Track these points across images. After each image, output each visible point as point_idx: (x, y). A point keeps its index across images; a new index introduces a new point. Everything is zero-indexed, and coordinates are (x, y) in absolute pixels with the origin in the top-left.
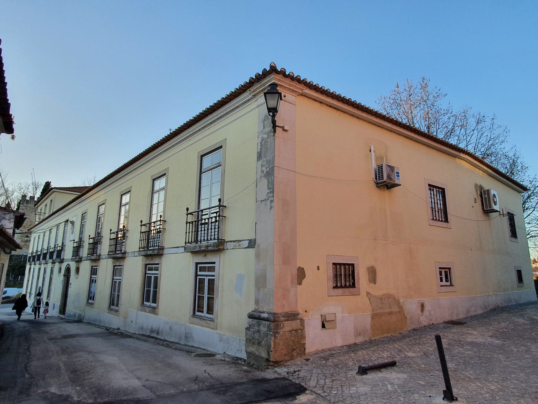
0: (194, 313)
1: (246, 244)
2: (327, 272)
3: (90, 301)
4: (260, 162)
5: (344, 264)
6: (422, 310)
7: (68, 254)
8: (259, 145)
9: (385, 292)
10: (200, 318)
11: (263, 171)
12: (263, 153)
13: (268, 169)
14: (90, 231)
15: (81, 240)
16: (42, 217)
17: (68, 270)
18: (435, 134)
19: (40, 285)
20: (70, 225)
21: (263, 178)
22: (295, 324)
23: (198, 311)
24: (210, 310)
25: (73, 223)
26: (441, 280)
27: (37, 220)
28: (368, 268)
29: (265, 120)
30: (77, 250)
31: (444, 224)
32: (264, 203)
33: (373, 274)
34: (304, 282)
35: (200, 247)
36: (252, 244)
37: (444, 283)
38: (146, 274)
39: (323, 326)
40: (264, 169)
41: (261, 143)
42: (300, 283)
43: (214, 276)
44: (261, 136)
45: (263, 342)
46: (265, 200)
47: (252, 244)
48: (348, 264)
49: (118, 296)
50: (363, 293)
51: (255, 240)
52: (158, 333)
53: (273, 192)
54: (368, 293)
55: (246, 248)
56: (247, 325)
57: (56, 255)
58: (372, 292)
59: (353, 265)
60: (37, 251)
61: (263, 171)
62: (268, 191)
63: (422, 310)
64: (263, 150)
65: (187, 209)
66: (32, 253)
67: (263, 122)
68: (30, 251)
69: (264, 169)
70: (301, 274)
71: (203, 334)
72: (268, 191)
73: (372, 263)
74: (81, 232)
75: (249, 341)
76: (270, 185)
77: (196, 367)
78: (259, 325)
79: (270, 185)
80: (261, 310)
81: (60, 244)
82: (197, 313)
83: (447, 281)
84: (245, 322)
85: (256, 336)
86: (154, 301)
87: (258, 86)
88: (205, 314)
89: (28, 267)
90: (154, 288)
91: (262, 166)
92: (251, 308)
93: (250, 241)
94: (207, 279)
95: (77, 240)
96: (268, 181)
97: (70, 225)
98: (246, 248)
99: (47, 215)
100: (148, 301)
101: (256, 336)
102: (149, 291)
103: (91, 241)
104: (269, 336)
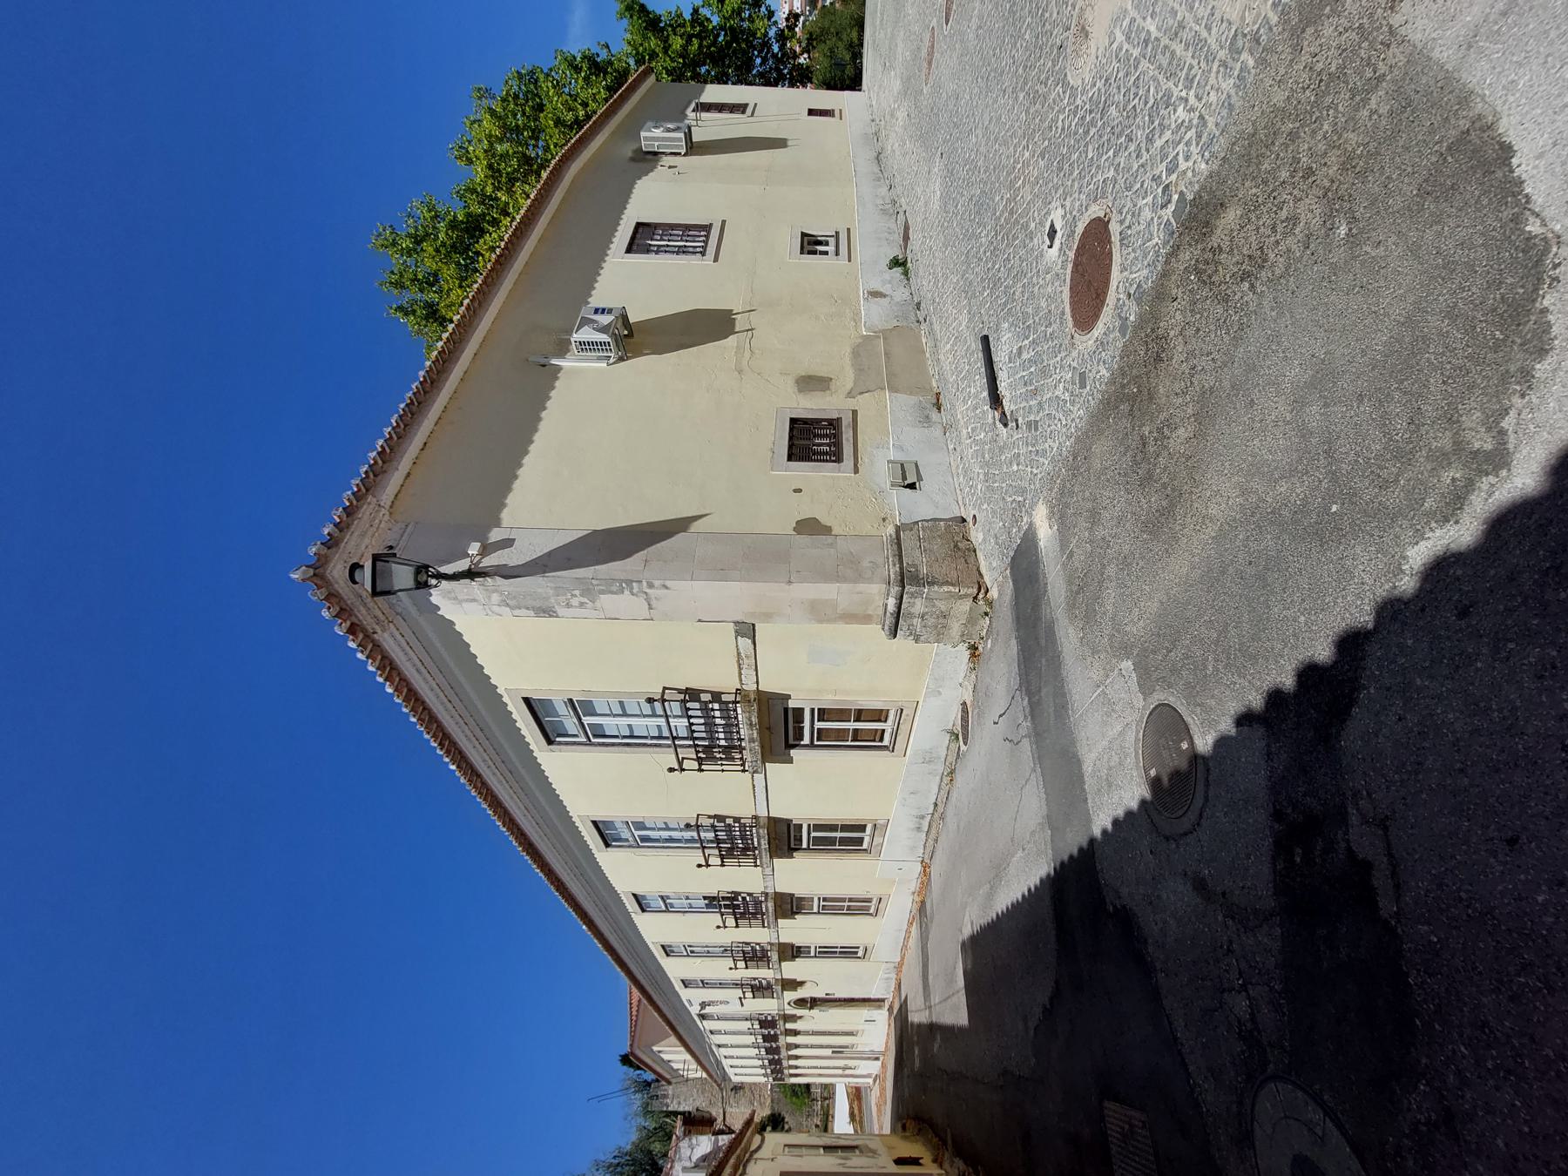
0: (886, 748)
1: (745, 643)
2: (804, 472)
3: (860, 954)
4: (560, 611)
5: (791, 438)
6: (882, 295)
7: (768, 1006)
8: (517, 612)
9: (847, 362)
10: (895, 735)
11: (582, 605)
12: (538, 604)
13: (577, 592)
14: (721, 969)
15: (739, 985)
16: (694, 1065)
17: (801, 1003)
18: (630, 284)
19: (828, 1052)
20: (708, 1010)
21: (598, 604)
22: (907, 539)
23: (881, 740)
24: (880, 715)
25: (703, 1005)
26: (826, 253)
27: (699, 1074)
28: (800, 391)
29: (455, 598)
30: (760, 989)
31: (715, 233)
32: (654, 603)
33: (811, 383)
34: (825, 520)
35: (752, 740)
36: (747, 630)
37: (831, 248)
38: (809, 848)
39: (912, 486)
40: (575, 602)
41: (512, 608)
42: (827, 530)
43: (812, 710)
44: (496, 608)
45: (943, 608)
46: (648, 600)
47: (747, 630)
48: (791, 429)
49: (851, 900)
50: (852, 404)
51: (736, 623)
52: (923, 817)
53: (629, 582)
54: (850, 395)
55: (754, 643)
56: (910, 642)
57: (770, 1030)
58: (849, 385)
59: (793, 421)
60: (763, 1067)
61: (582, 605)
62: (627, 592)
63: (882, 295)
64: (531, 603)
65: (671, 770)
66: (765, 1075)
67: (460, 602)
68: (763, 1080)
69: (575, 602)
70: (809, 527)
71: (927, 731)
72: (627, 592)
73: (790, 382)
74: (721, 985)
75: (940, 634)
76: (614, 588)
77: (987, 736)
78: (911, 615)
79: (614, 588)
80: (881, 612)
81: (748, 1024)
82: (886, 742)
83: (827, 244)
84: (903, 642)
85: (931, 621)
86: (862, 828)
87: (364, 611)
88: (888, 727)
89: (794, 1080)
90: (856, 731)
91: (568, 606)
92: (875, 633)
93: (738, 633)
94: (818, 725)
95: (739, 992)
96: (602, 592)
97: (708, 1010)
98: (754, 643)
99: (688, 1057)
100: (860, 841)
101: (931, 621)
102: (843, 841)
103: (741, 964)
104: (933, 595)
